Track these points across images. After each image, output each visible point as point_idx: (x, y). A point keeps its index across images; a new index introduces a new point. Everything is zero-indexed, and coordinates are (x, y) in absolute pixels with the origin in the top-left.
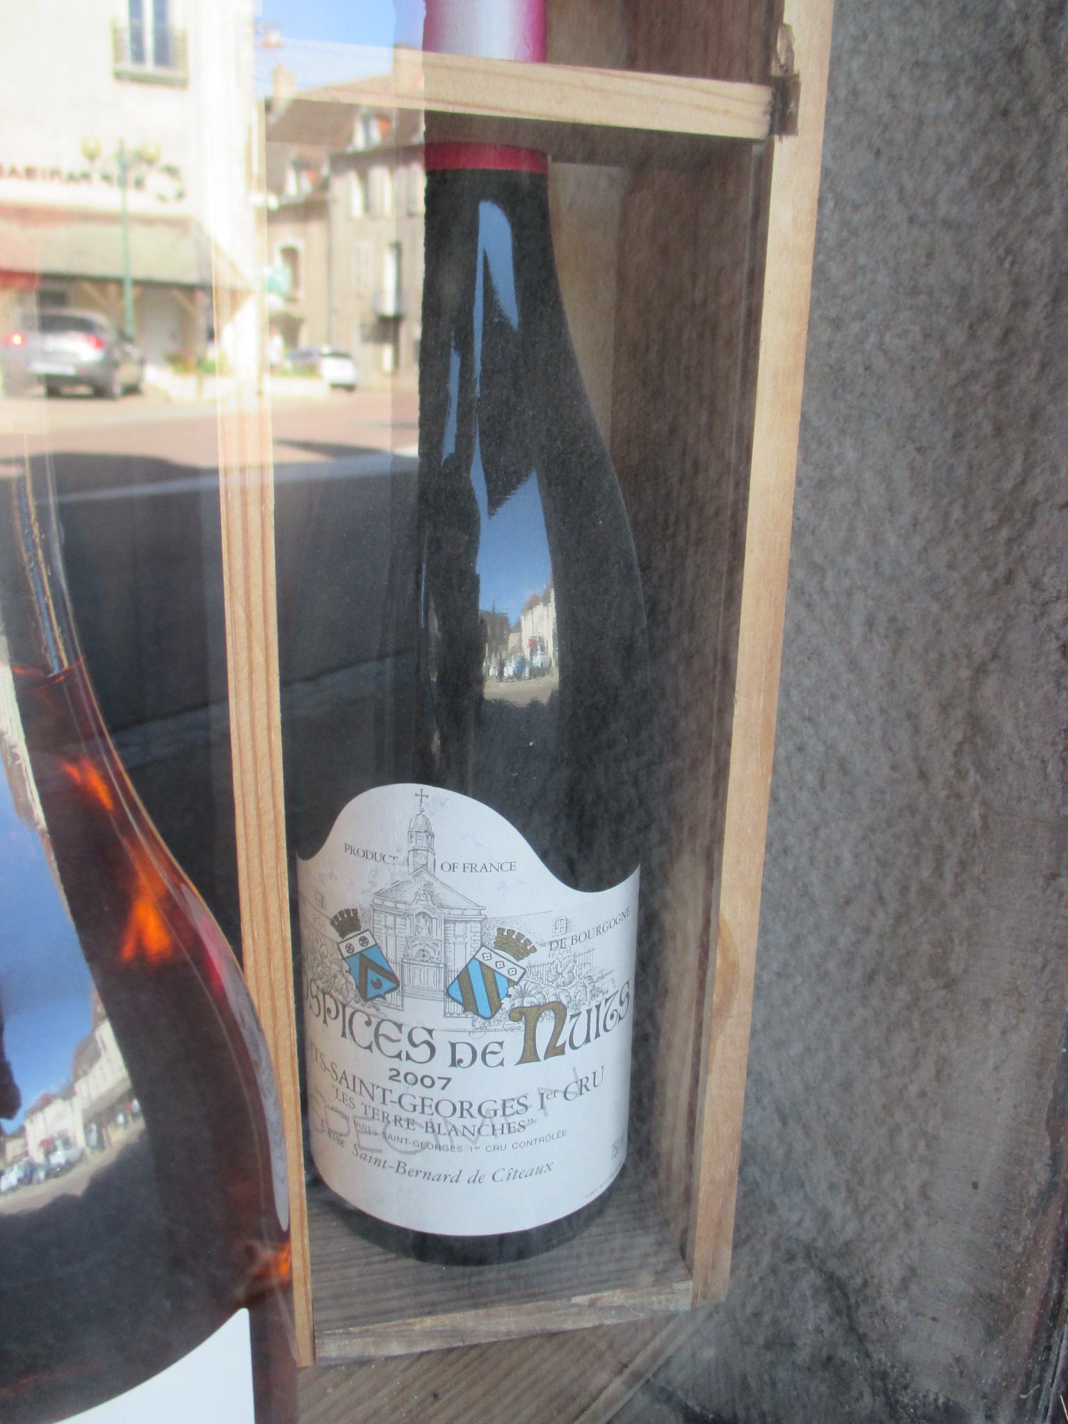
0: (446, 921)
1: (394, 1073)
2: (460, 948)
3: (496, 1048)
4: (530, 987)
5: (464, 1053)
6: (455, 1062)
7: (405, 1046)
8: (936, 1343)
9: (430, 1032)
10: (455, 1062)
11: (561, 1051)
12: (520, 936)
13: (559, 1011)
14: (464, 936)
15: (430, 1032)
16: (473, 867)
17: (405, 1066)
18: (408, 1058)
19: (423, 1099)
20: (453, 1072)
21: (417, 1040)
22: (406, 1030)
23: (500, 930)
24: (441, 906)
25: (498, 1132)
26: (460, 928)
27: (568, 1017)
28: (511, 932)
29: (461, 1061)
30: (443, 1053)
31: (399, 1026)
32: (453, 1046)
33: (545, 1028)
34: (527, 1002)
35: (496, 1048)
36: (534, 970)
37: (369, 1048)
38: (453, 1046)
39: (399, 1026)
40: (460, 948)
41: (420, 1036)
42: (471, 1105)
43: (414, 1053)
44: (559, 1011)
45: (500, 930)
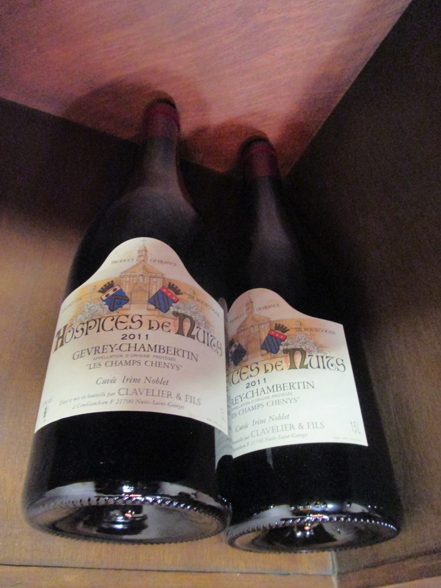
0: (259, 325)
1: (125, 336)
2: (154, 287)
4: (289, 342)
5: (154, 325)
6: (151, 328)
7: (130, 324)
9: (141, 316)
10: (151, 328)
12: (283, 326)
14: (265, 328)
15: (141, 316)
17: (128, 332)
18: (130, 328)
19: (168, 347)
20: (150, 333)
21: (134, 320)
22: (130, 318)
23: (276, 324)
24: (257, 321)
25: (154, 365)
26: (155, 280)
27: (307, 356)
28: (279, 325)
29: (153, 327)
31: (127, 316)
32: (150, 321)
34: (289, 347)
36: (290, 337)
37: (112, 330)
38: (150, 321)
39: (127, 316)
41: (340, 362)
42: (99, 348)
43: (133, 325)
45: (276, 324)
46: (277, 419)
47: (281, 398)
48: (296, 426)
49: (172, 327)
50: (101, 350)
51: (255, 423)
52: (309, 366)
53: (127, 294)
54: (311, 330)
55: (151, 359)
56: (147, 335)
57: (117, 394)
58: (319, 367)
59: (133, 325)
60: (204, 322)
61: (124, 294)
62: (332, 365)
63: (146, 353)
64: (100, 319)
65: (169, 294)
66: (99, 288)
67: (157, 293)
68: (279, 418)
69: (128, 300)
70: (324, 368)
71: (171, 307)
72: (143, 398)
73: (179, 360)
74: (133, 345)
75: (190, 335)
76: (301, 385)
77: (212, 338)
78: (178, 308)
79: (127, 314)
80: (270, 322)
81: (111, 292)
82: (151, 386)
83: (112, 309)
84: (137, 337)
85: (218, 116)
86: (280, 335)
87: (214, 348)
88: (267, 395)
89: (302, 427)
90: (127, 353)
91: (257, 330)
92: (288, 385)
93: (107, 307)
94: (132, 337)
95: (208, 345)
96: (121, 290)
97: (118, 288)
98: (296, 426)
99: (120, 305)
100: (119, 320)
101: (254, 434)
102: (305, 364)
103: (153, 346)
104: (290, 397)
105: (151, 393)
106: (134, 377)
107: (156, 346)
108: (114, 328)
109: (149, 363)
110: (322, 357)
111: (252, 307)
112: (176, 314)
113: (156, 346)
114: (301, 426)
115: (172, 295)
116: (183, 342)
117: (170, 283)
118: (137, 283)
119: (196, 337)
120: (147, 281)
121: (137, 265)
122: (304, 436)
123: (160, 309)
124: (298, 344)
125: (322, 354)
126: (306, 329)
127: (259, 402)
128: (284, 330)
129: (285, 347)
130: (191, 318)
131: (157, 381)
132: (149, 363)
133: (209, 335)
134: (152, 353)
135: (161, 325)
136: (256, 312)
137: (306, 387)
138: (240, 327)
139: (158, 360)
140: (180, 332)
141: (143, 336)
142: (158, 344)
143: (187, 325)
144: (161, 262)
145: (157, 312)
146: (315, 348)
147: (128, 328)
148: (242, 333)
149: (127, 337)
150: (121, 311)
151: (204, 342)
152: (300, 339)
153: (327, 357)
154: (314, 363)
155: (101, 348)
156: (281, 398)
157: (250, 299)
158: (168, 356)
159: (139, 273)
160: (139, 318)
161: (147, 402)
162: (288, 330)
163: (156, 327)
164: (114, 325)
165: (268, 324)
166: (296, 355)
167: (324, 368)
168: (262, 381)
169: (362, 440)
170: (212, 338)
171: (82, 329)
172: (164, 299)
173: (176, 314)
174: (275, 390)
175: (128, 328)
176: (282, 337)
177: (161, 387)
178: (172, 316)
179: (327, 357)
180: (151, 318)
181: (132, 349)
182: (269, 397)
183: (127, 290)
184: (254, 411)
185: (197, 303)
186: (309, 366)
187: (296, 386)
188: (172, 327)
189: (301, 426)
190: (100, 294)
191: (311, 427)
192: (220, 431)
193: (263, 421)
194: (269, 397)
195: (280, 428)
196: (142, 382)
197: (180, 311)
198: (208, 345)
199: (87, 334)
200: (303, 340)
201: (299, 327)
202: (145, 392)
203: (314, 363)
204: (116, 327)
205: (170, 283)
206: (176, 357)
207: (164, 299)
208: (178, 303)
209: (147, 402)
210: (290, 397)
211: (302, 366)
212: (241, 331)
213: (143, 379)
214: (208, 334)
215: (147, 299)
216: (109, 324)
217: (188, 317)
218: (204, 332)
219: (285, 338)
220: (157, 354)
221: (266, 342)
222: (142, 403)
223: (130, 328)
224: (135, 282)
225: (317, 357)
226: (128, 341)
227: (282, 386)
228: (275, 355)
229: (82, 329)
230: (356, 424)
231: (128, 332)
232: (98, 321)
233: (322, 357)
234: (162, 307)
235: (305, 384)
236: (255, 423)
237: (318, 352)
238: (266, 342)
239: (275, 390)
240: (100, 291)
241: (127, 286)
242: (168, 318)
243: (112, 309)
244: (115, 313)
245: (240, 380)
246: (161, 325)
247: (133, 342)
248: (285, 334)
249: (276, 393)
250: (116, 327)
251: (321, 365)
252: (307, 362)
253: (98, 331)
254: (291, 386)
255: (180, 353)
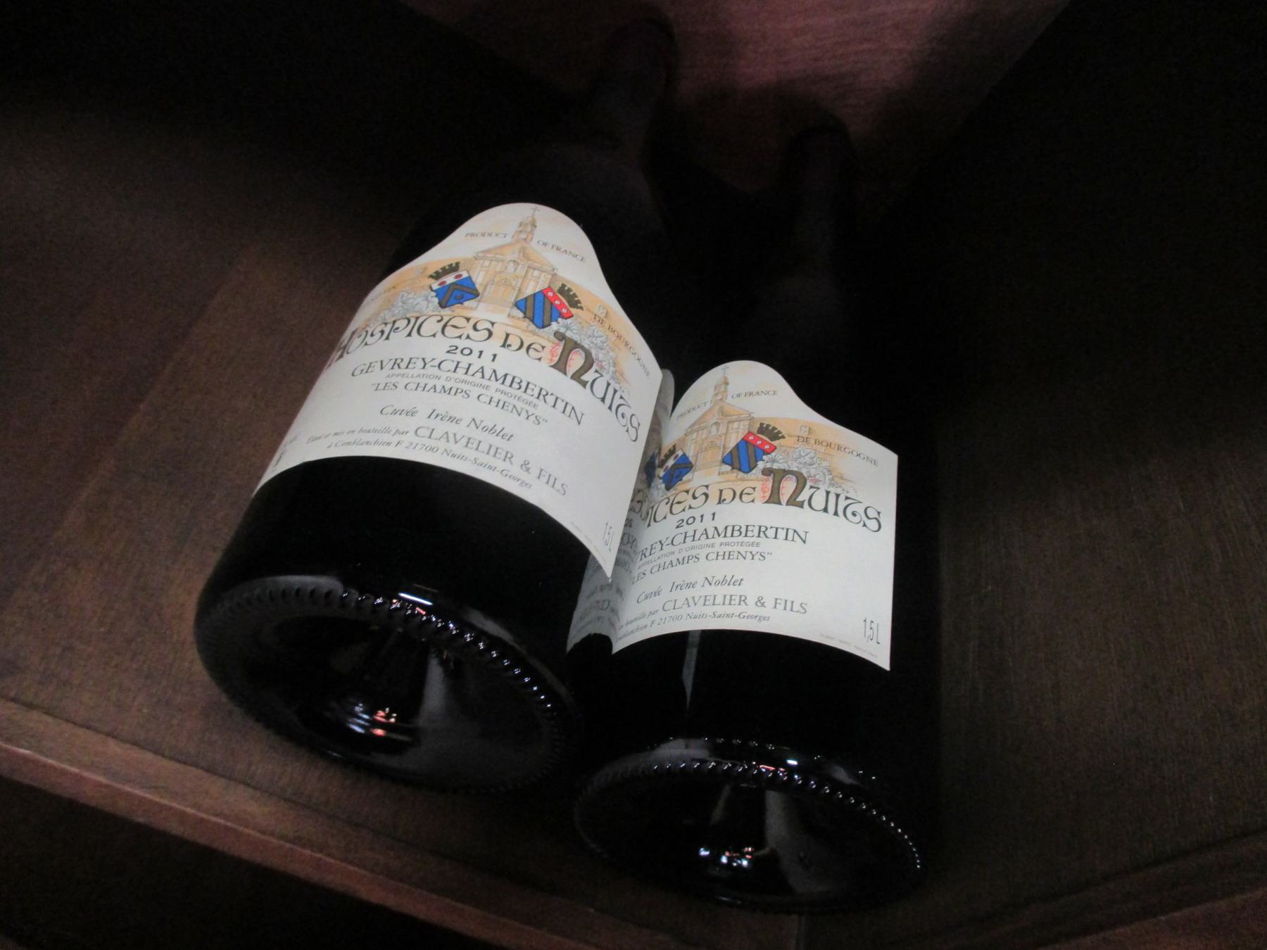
2: (532, 283)
3: (750, 491)
4: (779, 457)
5: (728, 495)
8: (618, 647)
9: (493, 324)
11: (801, 505)
12: (774, 428)
13: (801, 481)
15: (493, 324)
16: (751, 394)
17: (462, 343)
18: (468, 337)
20: (502, 353)
21: (479, 327)
22: (472, 322)
25: (493, 404)
26: (536, 273)
30: (714, 497)
31: (468, 320)
32: (508, 335)
33: (788, 486)
34: (775, 466)
35: (750, 491)
38: (508, 335)
39: (468, 320)
40: (532, 283)
41: (871, 513)
44: (801, 481)
46: (718, 583)
47: (736, 548)
48: (751, 600)
49: (545, 354)
50: (403, 365)
51: (675, 587)
52: (806, 504)
53: (477, 286)
54: (829, 445)
55: (491, 392)
56: (495, 356)
57: (412, 433)
58: (825, 510)
59: (472, 333)
60: (612, 369)
61: (474, 284)
62: (854, 514)
63: (485, 382)
64: (417, 318)
65: (557, 302)
66: (431, 272)
67: (534, 295)
68: (723, 582)
69: (477, 295)
70: (836, 514)
71: (554, 324)
72: (458, 449)
73: (543, 409)
74: (464, 365)
75: (577, 377)
76: (782, 534)
77: (622, 402)
78: (568, 328)
79: (469, 315)
80: (752, 419)
81: (450, 279)
82: (478, 435)
83: (443, 305)
84: (476, 353)
85: (757, 69)
86: (765, 443)
87: (624, 421)
88: (710, 541)
89: (763, 605)
90: (450, 374)
91: (723, 429)
92: (756, 530)
93: (436, 300)
94: (467, 352)
95: (610, 408)
96: (470, 278)
97: (465, 275)
98: (751, 600)
99: (460, 301)
100: (451, 323)
101: (670, 606)
102: (800, 499)
103: (500, 375)
104: (754, 549)
105: (475, 446)
106: (452, 413)
107: (506, 375)
108: (439, 334)
109: (485, 399)
110: (838, 496)
111: (726, 391)
112: (560, 336)
113: (506, 375)
114: (760, 602)
115: (562, 304)
116: (563, 385)
117: (563, 286)
118: (500, 272)
119: (588, 386)
120: (521, 271)
121: (510, 245)
122: (762, 618)
123: (532, 321)
124: (795, 464)
125: (839, 491)
126: (818, 442)
127: (694, 552)
128: (775, 435)
129: (769, 465)
130: (588, 355)
131: (492, 430)
132: (485, 399)
133: (618, 395)
134: (495, 385)
135: (526, 345)
136: (729, 400)
137: (790, 537)
138: (693, 425)
139: (503, 398)
140: (561, 366)
141: (487, 356)
142: (512, 372)
143: (576, 361)
144: (558, 249)
145: (527, 323)
146: (829, 477)
147: (464, 337)
148: (695, 435)
149: (458, 351)
150: (458, 309)
151: (603, 400)
152: (801, 456)
153: (847, 498)
154: (819, 501)
155: (406, 361)
156: (736, 548)
157: (726, 379)
158: (525, 396)
159: (510, 257)
160: (489, 326)
161: (462, 457)
162: (783, 437)
163: (516, 344)
164: (440, 329)
165: (747, 423)
166: (787, 487)
167: (836, 514)
168: (708, 517)
169: (881, 656)
170: (622, 402)
171: (382, 332)
172: (544, 308)
173: (560, 336)
174: (729, 533)
175: (464, 337)
176: (767, 447)
177: (497, 441)
178: (552, 337)
179: (847, 498)
180: (510, 330)
181: (461, 371)
182: (713, 545)
183: (479, 280)
184: (680, 566)
185: (608, 333)
186: (806, 504)
187: (771, 533)
188: (545, 354)
189: (760, 602)
190: (432, 281)
191: (781, 607)
192: (599, 567)
193: (691, 585)
194: (713, 545)
195: (719, 600)
196: (464, 424)
197: (569, 334)
198: (610, 408)
199: (387, 338)
200: (807, 459)
201: (805, 435)
202: (464, 441)
203: (819, 501)
204: (443, 332)
205: (563, 286)
206: (540, 403)
207: (544, 308)
208: (569, 321)
209: (462, 457)
210: (754, 549)
211: (792, 501)
212: (691, 433)
213: (467, 420)
214: (615, 391)
215: (513, 300)
216: (431, 326)
217: (582, 348)
218: (609, 384)
219: (774, 448)
220: (506, 388)
221: (735, 453)
222: (454, 456)
223: (468, 337)
224: (498, 269)
225: (828, 493)
226: (458, 357)
227: (743, 530)
228: (745, 476)
229: (382, 332)
230: (874, 626)
231: (462, 343)
232: (413, 321)
233: (838, 496)
234: (537, 320)
235: (791, 533)
236: (675, 587)
237: (832, 485)
238: (735, 453)
239: (729, 533)
240: (431, 276)
241: (482, 274)
242: (545, 338)
243: (443, 305)
244: (446, 312)
245: (669, 516)
246: (526, 345)
247: (465, 361)
248: (775, 443)
249: (729, 540)
250: (443, 332)
251: (831, 508)
252: (804, 496)
253: (409, 335)
254: (762, 531)
255: (550, 400)
